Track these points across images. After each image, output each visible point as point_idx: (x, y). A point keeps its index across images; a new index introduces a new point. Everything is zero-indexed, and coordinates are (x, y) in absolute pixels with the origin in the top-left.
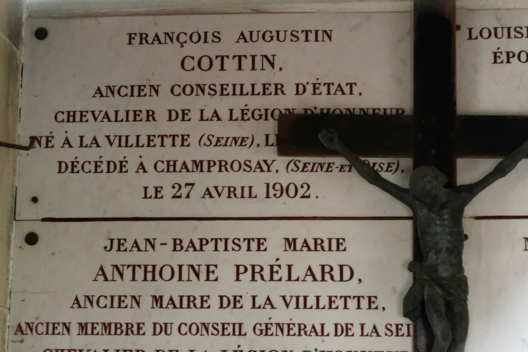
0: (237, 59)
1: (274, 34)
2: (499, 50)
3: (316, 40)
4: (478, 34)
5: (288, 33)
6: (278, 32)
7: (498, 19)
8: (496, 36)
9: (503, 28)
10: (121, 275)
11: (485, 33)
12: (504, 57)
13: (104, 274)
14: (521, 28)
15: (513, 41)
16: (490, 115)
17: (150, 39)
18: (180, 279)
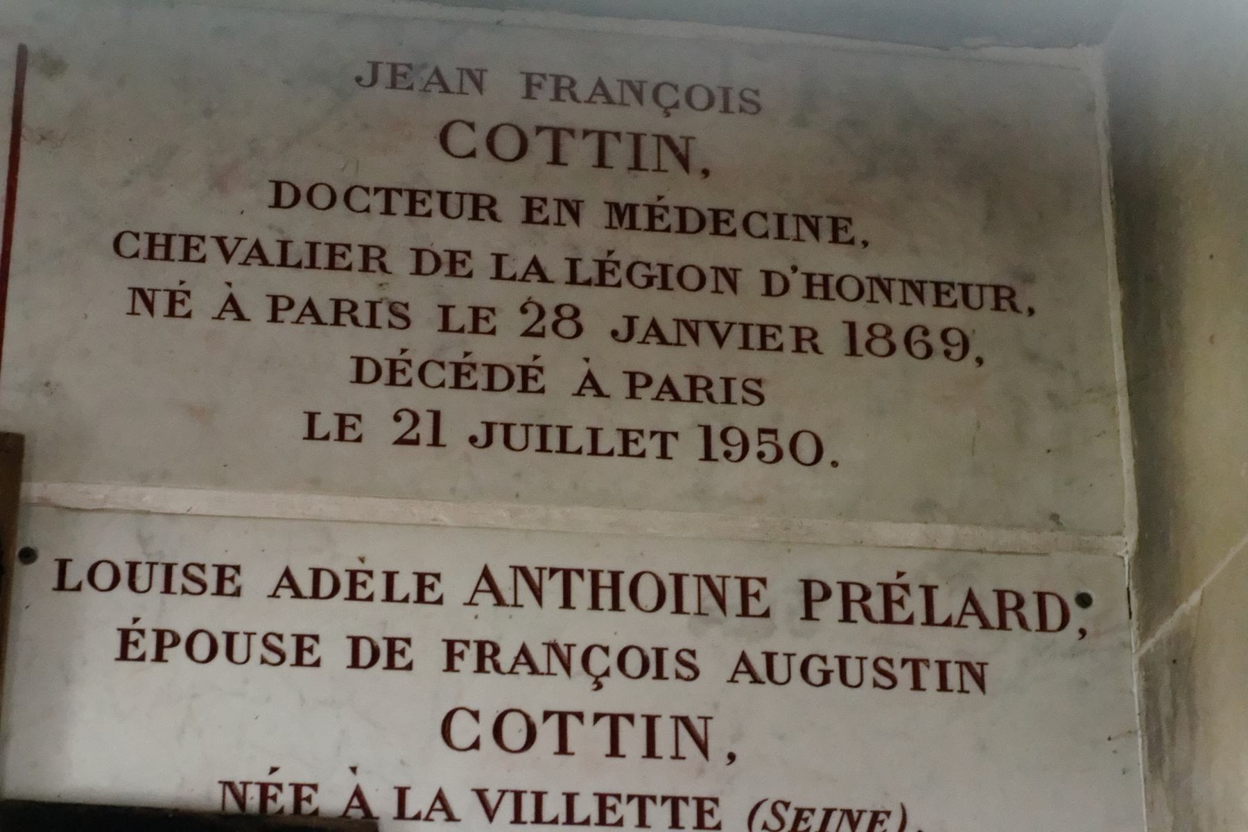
0: (605, 723)
1: (833, 665)
2: (138, 626)
3: (943, 687)
4: (84, 577)
5: (868, 665)
6: (842, 661)
7: (143, 541)
8: (132, 585)
9: (152, 564)
10: (538, 593)
11: (104, 576)
12: (148, 645)
13: (494, 589)
14: (202, 567)
15: (176, 601)
16: (91, 802)
17: (506, 660)
18: (679, 609)
